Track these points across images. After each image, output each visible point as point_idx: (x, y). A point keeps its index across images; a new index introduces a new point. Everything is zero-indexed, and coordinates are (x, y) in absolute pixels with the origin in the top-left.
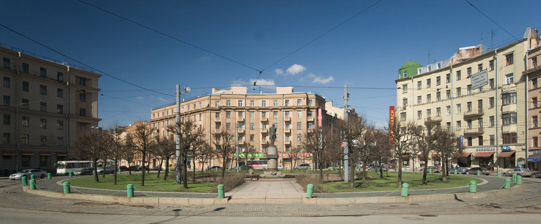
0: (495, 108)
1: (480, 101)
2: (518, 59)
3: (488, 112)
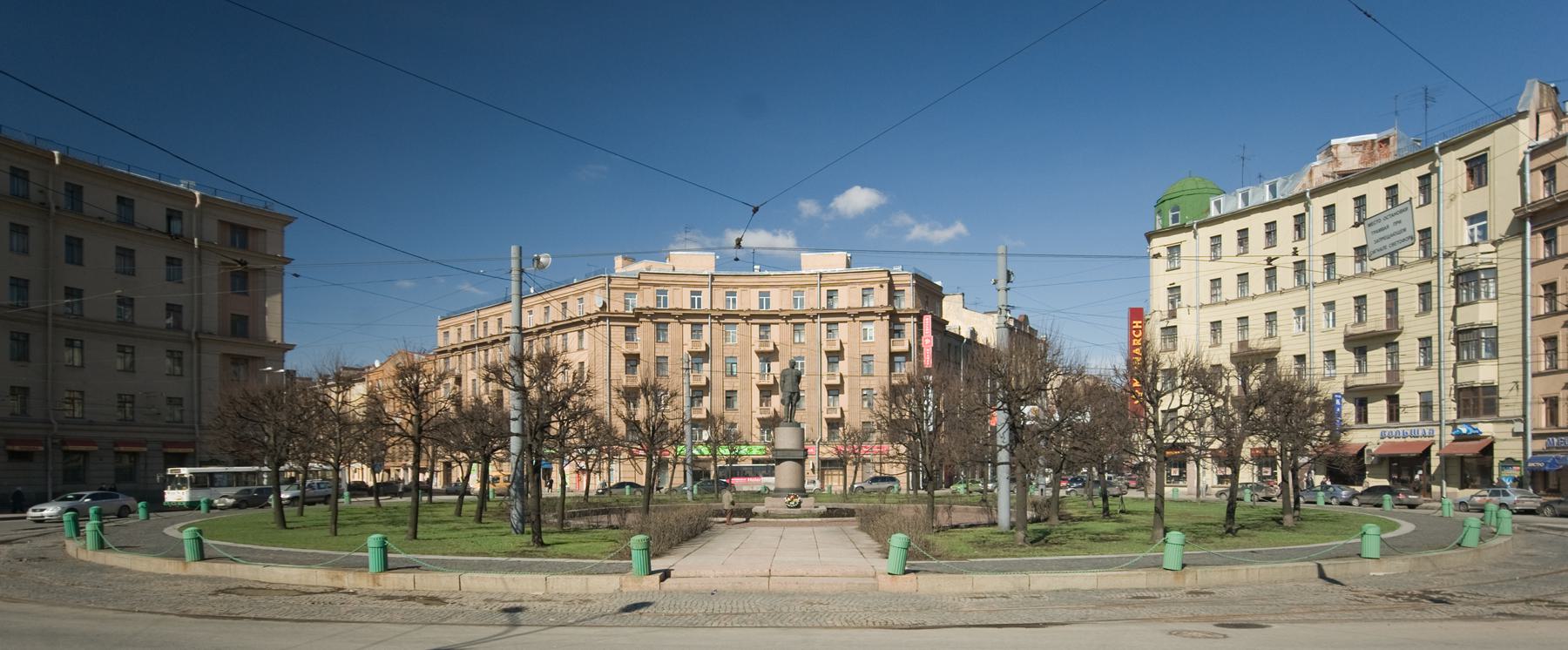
0: (1434, 312)
1: (1392, 294)
2: (1502, 170)
3: (1414, 325)
